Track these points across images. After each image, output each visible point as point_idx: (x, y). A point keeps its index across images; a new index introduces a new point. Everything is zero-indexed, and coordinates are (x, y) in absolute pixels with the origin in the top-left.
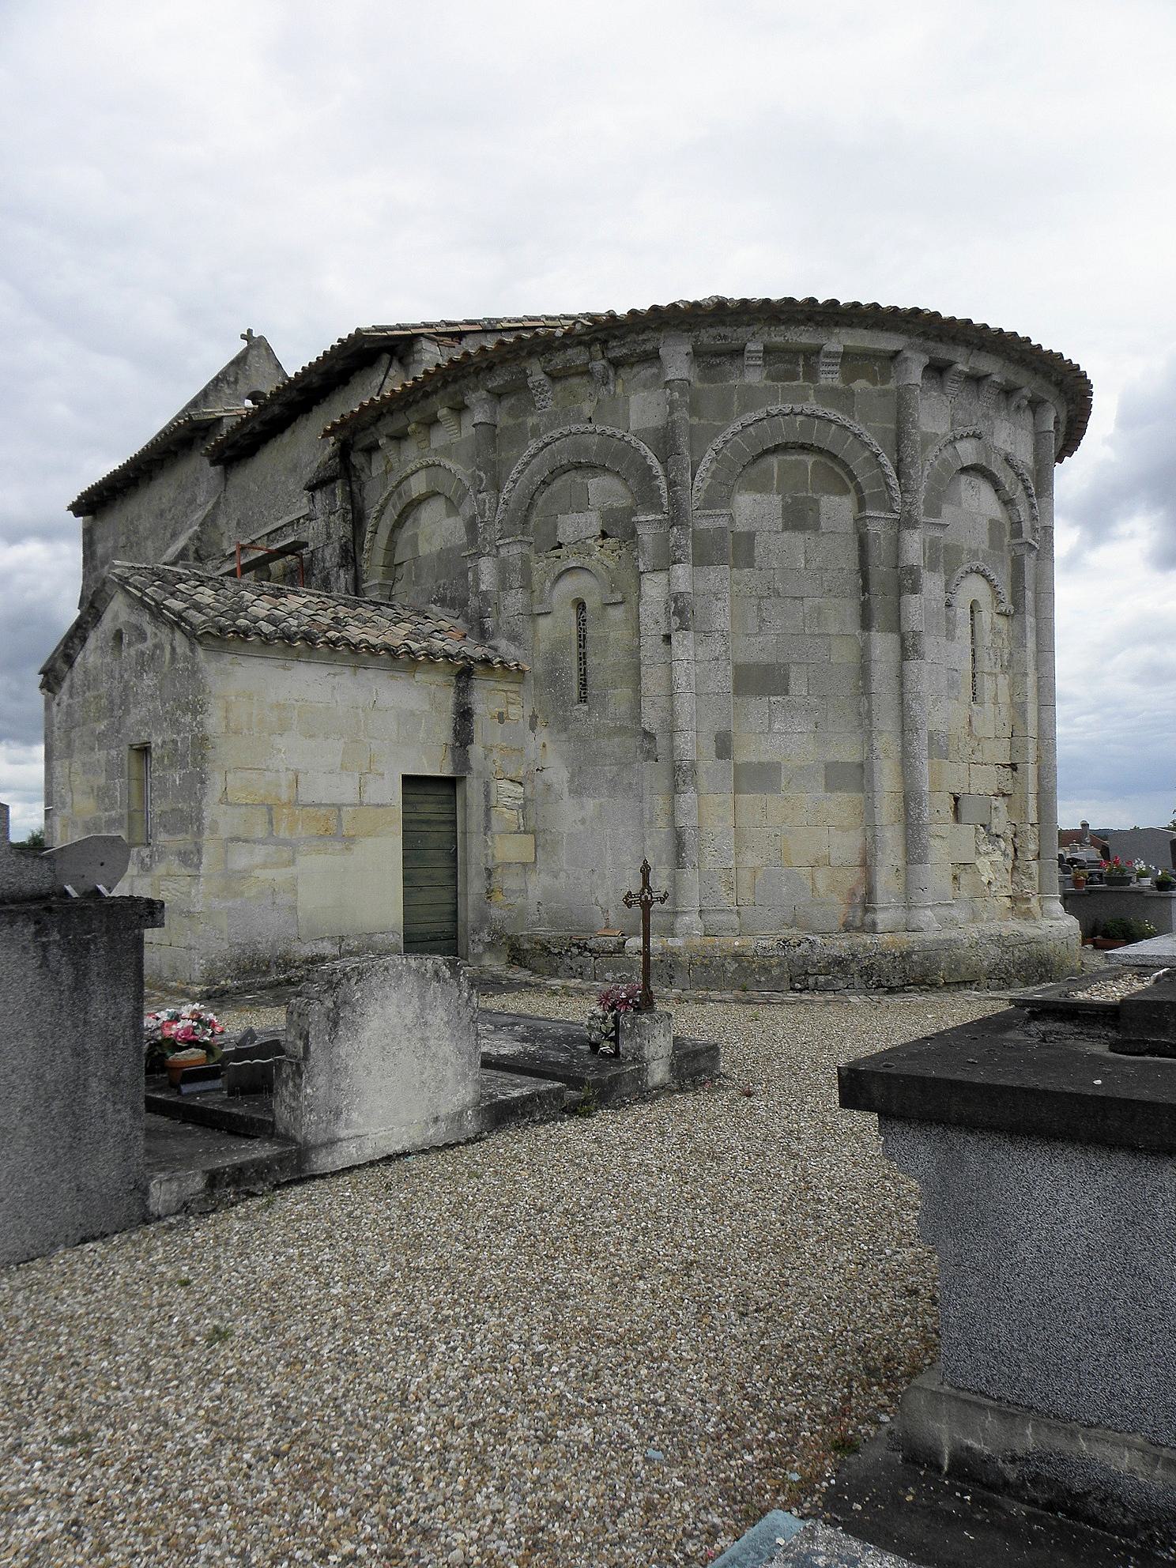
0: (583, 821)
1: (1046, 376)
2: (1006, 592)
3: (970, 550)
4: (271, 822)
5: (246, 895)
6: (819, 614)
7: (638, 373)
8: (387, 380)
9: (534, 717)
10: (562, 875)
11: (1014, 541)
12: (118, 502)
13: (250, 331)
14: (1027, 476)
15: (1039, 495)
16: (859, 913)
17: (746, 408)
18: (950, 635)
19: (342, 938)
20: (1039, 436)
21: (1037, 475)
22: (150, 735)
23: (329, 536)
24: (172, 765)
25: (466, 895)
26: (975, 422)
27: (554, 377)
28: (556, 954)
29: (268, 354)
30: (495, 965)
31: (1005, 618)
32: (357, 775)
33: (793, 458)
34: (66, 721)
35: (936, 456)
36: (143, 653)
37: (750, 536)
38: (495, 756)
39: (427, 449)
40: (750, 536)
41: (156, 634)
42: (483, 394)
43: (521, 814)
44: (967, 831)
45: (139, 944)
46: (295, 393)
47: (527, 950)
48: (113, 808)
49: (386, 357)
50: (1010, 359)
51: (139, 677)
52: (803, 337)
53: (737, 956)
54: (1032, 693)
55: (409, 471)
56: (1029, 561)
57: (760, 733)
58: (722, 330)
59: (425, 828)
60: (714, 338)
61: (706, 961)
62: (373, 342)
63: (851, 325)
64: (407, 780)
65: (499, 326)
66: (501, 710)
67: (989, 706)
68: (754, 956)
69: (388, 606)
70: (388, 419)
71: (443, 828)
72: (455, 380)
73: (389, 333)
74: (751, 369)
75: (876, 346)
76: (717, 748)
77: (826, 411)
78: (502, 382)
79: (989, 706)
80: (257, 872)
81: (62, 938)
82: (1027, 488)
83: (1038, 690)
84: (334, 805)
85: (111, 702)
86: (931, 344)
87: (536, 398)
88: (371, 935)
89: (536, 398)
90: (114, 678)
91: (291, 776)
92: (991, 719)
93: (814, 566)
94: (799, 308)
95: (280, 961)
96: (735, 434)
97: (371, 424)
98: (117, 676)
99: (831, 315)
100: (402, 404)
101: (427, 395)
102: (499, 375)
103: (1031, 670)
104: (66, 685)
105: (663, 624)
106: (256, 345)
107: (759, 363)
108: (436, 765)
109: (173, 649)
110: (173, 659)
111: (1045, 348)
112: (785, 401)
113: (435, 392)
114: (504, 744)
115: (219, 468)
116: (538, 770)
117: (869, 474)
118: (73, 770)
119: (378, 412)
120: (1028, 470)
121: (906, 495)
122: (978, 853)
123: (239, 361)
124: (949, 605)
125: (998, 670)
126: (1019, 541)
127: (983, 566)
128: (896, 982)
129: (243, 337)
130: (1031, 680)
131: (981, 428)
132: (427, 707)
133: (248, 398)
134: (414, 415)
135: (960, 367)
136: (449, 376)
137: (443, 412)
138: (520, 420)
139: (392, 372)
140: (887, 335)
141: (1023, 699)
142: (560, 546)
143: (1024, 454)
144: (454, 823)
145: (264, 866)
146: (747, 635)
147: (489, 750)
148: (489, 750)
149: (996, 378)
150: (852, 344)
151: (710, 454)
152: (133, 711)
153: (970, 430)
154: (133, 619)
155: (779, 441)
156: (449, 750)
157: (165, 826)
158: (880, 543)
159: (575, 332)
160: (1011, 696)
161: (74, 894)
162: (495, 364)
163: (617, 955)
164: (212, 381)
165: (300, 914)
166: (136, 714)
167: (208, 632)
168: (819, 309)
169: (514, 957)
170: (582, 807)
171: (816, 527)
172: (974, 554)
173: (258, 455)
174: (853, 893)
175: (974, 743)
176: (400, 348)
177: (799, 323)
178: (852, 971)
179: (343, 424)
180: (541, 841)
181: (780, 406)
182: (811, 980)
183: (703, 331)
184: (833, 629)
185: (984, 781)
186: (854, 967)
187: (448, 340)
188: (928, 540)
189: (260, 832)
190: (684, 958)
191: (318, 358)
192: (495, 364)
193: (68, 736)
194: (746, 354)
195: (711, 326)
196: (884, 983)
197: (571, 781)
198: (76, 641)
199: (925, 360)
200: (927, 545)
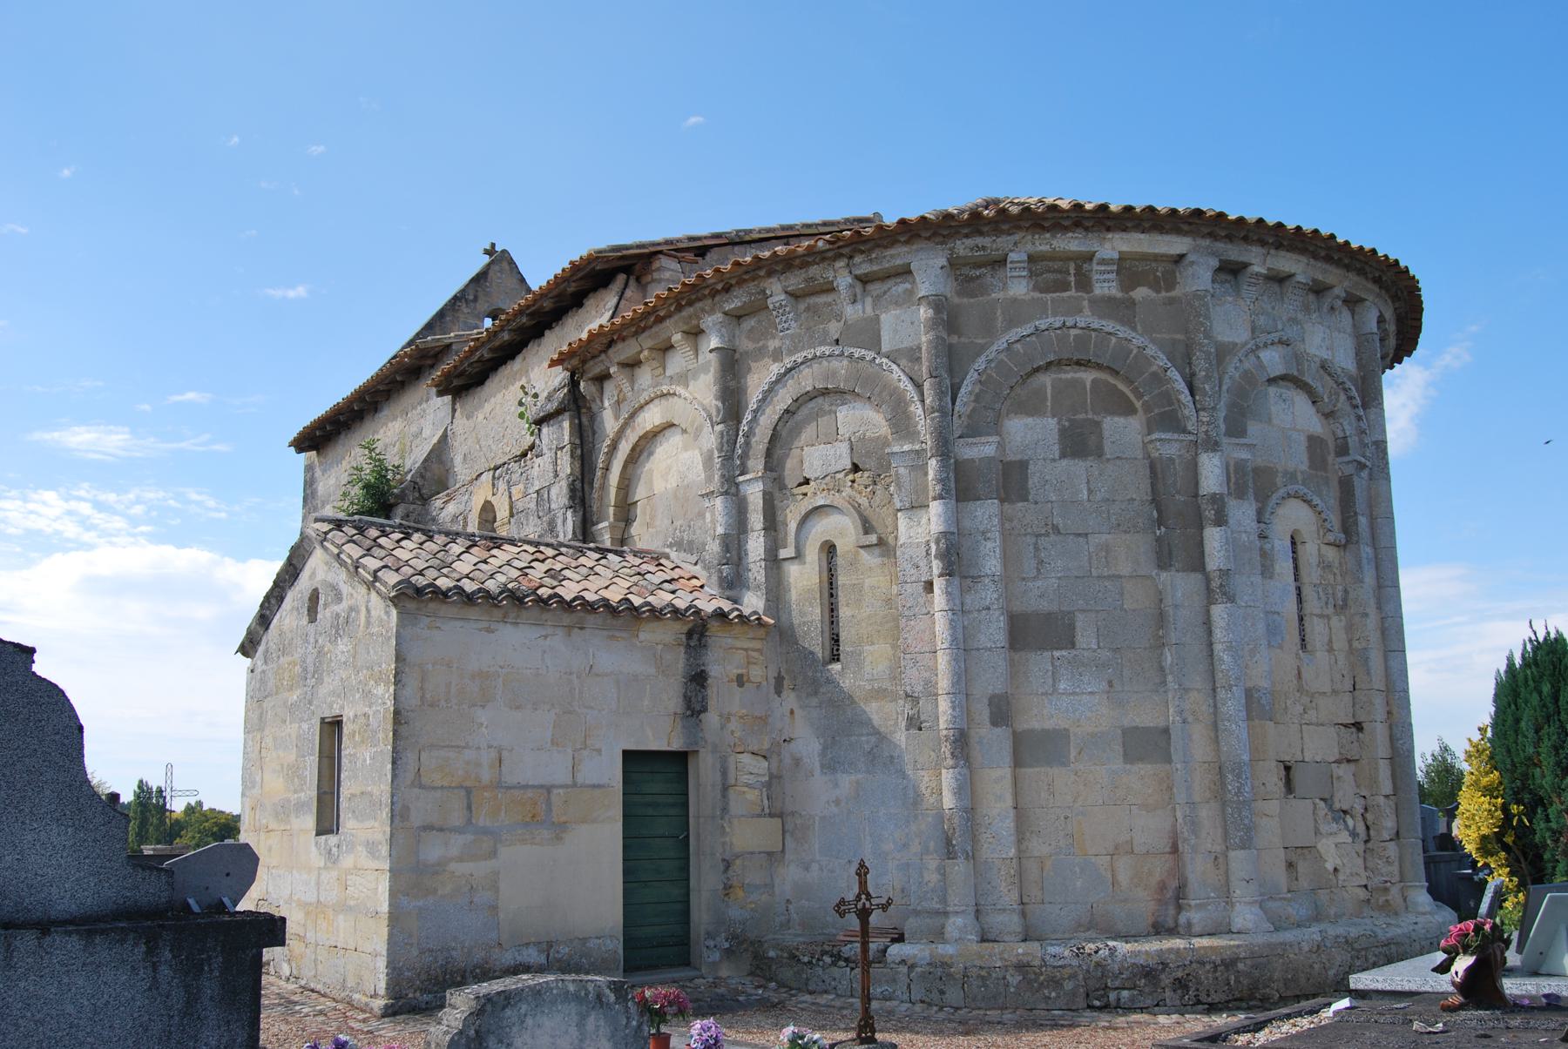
0: (837, 802)
1: (1361, 272)
2: (1334, 519)
3: (1286, 473)
4: (469, 808)
5: (440, 892)
6: (1107, 552)
7: (889, 289)
8: (623, 302)
9: (779, 680)
10: (815, 867)
11: (1340, 460)
12: (342, 436)
13: (493, 245)
14: (1349, 385)
15: (1365, 406)
16: (1172, 911)
17: (1011, 323)
18: (1267, 571)
19: (550, 944)
20: (1360, 340)
21: (1363, 383)
22: (342, 707)
23: (556, 475)
24: (363, 742)
25: (699, 891)
26: (1280, 327)
27: (795, 296)
28: (805, 964)
29: (511, 269)
30: (732, 975)
31: (1336, 549)
32: (570, 751)
33: (1069, 376)
34: (260, 689)
35: (1236, 368)
36: (338, 615)
37: (1023, 465)
38: (734, 725)
39: (661, 377)
40: (1023, 465)
41: (352, 595)
42: (719, 316)
43: (765, 794)
44: (1301, 808)
45: (257, 966)
46: (524, 320)
47: (772, 958)
48: (302, 790)
49: (621, 278)
50: (1315, 256)
51: (334, 641)
52: (1071, 243)
53: (1022, 967)
54: (1374, 637)
55: (642, 401)
56: (1360, 483)
57: (1042, 694)
58: (979, 241)
59: (650, 811)
60: (972, 249)
61: (983, 973)
62: (608, 261)
63: (1125, 230)
64: (628, 755)
65: (747, 238)
66: (740, 671)
67: (1321, 656)
68: (1041, 966)
69: (616, 553)
70: (620, 346)
71: (672, 811)
72: (690, 304)
73: (625, 252)
74: (1015, 281)
75: (1156, 251)
76: (991, 713)
77: (1104, 323)
78: (739, 304)
79: (1321, 656)
80: (453, 866)
81: (174, 957)
82: (1350, 398)
83: (1383, 633)
84: (542, 787)
85: (305, 670)
86: (1220, 245)
87: (777, 320)
88: (584, 940)
89: (777, 320)
90: (309, 643)
91: (493, 754)
92: (1322, 670)
93: (1098, 496)
94: (1065, 215)
95: (478, 971)
96: (999, 352)
97: (601, 352)
98: (312, 640)
99: (1102, 219)
100: (634, 330)
101: (660, 320)
102: (736, 297)
103: (1372, 610)
104: (261, 649)
105: (924, 569)
106: (500, 260)
107: (1024, 273)
108: (660, 737)
109: (368, 611)
110: (368, 623)
111: (1354, 245)
112: (1055, 315)
113: (669, 316)
114: (744, 711)
115: (448, 399)
116: (785, 741)
117: (1156, 392)
118: (263, 745)
119: (606, 341)
120: (1351, 378)
121: (1202, 413)
122: (1317, 832)
123: (480, 279)
124: (1262, 536)
125: (1330, 610)
126: (1346, 459)
127: (1303, 490)
128: (1215, 998)
129: (487, 252)
130: (1372, 622)
131: (1291, 332)
132: (652, 671)
133: (488, 317)
134: (647, 341)
135: (1256, 269)
136: (683, 299)
137: (677, 338)
138: (761, 343)
139: (628, 293)
140: (1167, 238)
141: (1364, 645)
142: (807, 482)
143: (1344, 360)
144: (686, 805)
145: (461, 859)
146: (1024, 579)
147: (726, 718)
148: (726, 718)
149: (1300, 278)
150: (1128, 250)
151: (972, 376)
152: (326, 679)
153: (1275, 336)
154: (331, 577)
155: (1052, 357)
156: (678, 720)
157: (354, 812)
158: (1175, 468)
159: (817, 250)
160: (1350, 641)
161: (196, 908)
162: (731, 285)
163: (877, 965)
164: (450, 301)
165: (502, 916)
166: (330, 684)
167: (403, 593)
168: (1087, 215)
169: (758, 967)
170: (836, 785)
171: (1099, 453)
172: (1291, 477)
173: (488, 383)
174: (1162, 887)
175: (1306, 700)
176: (637, 267)
177: (1066, 229)
178: (1163, 985)
179: (571, 354)
180: (789, 827)
181: (1051, 320)
182: (1112, 996)
183: (958, 242)
184: (1124, 569)
185: (1320, 746)
186: (1166, 980)
187: (690, 256)
188: (1232, 463)
189: (457, 819)
190: (957, 969)
191: (548, 282)
192: (731, 285)
193: (260, 707)
194: (1009, 265)
195: (967, 236)
196: (1203, 998)
197: (823, 753)
198: (273, 601)
199: (1215, 263)
200: (1232, 469)
